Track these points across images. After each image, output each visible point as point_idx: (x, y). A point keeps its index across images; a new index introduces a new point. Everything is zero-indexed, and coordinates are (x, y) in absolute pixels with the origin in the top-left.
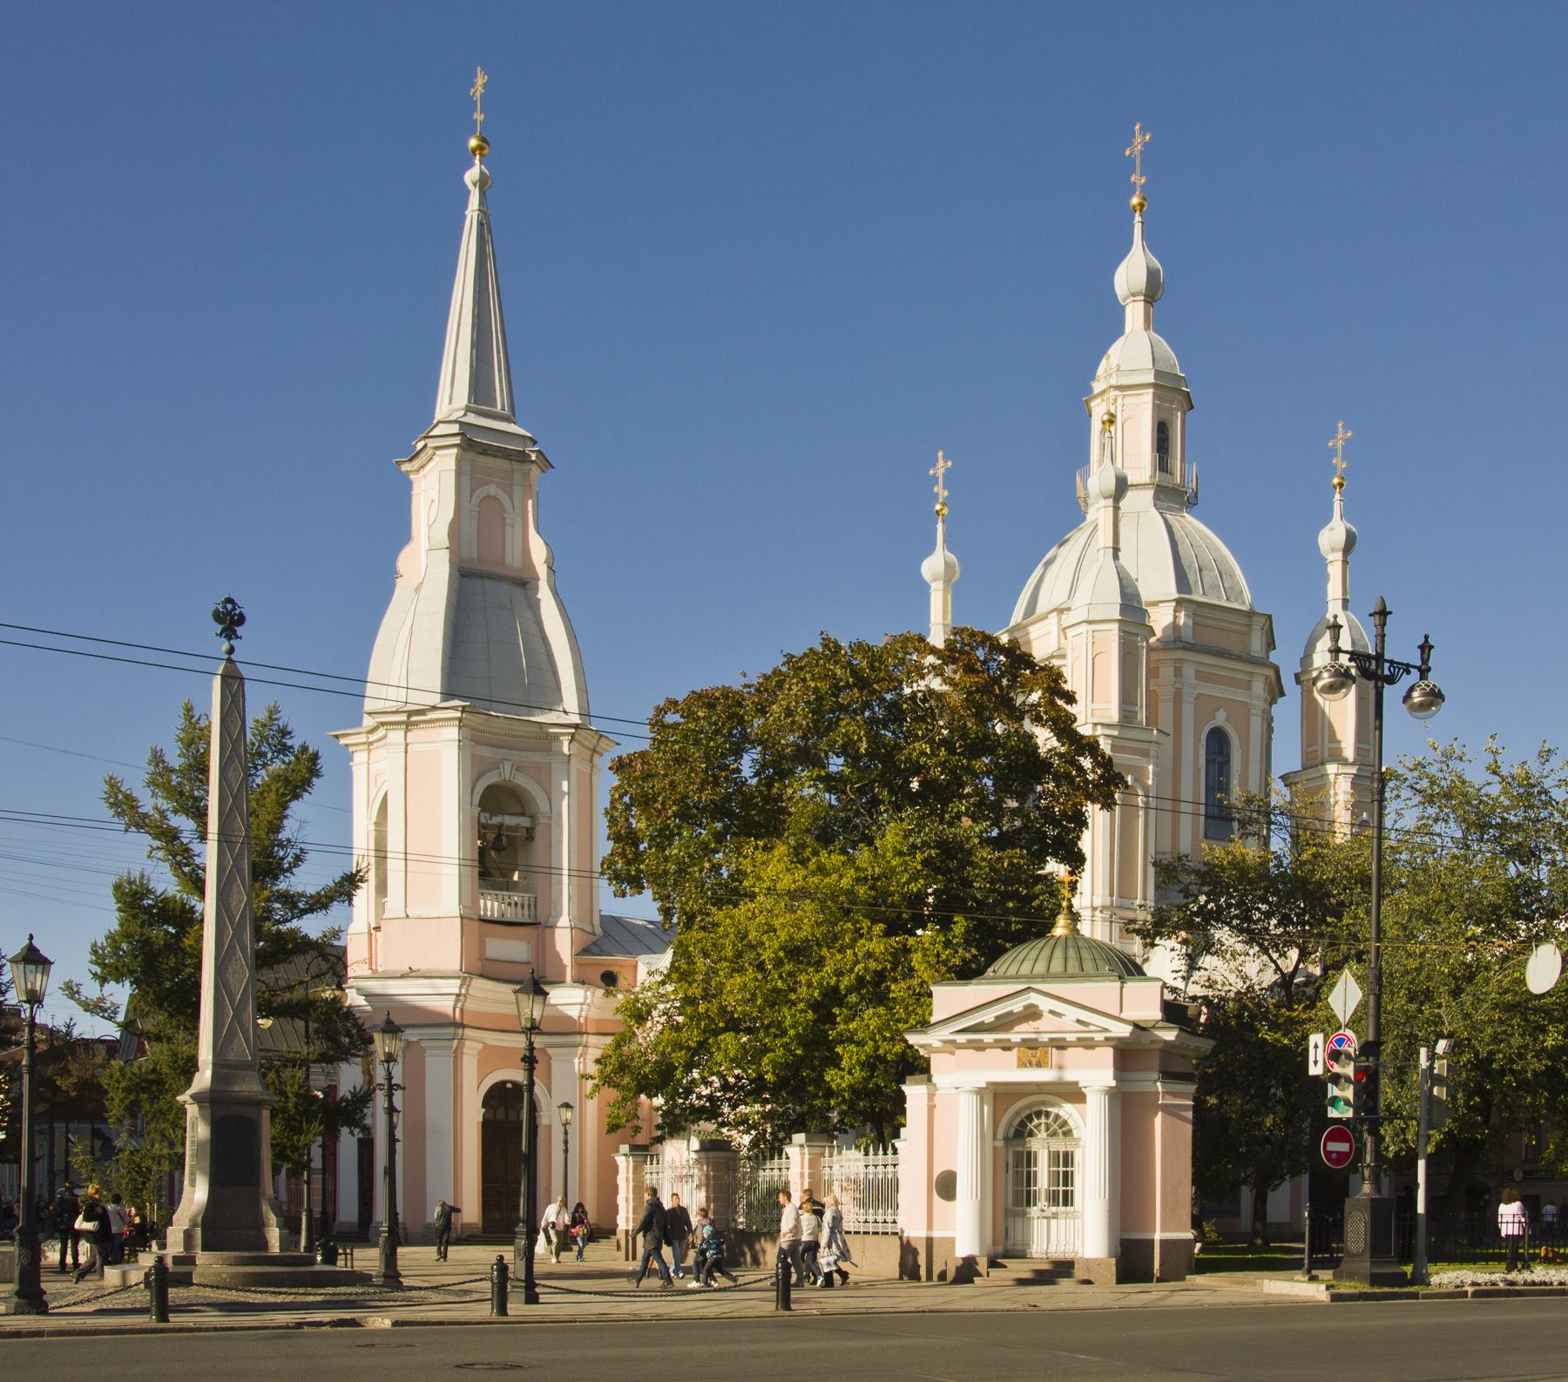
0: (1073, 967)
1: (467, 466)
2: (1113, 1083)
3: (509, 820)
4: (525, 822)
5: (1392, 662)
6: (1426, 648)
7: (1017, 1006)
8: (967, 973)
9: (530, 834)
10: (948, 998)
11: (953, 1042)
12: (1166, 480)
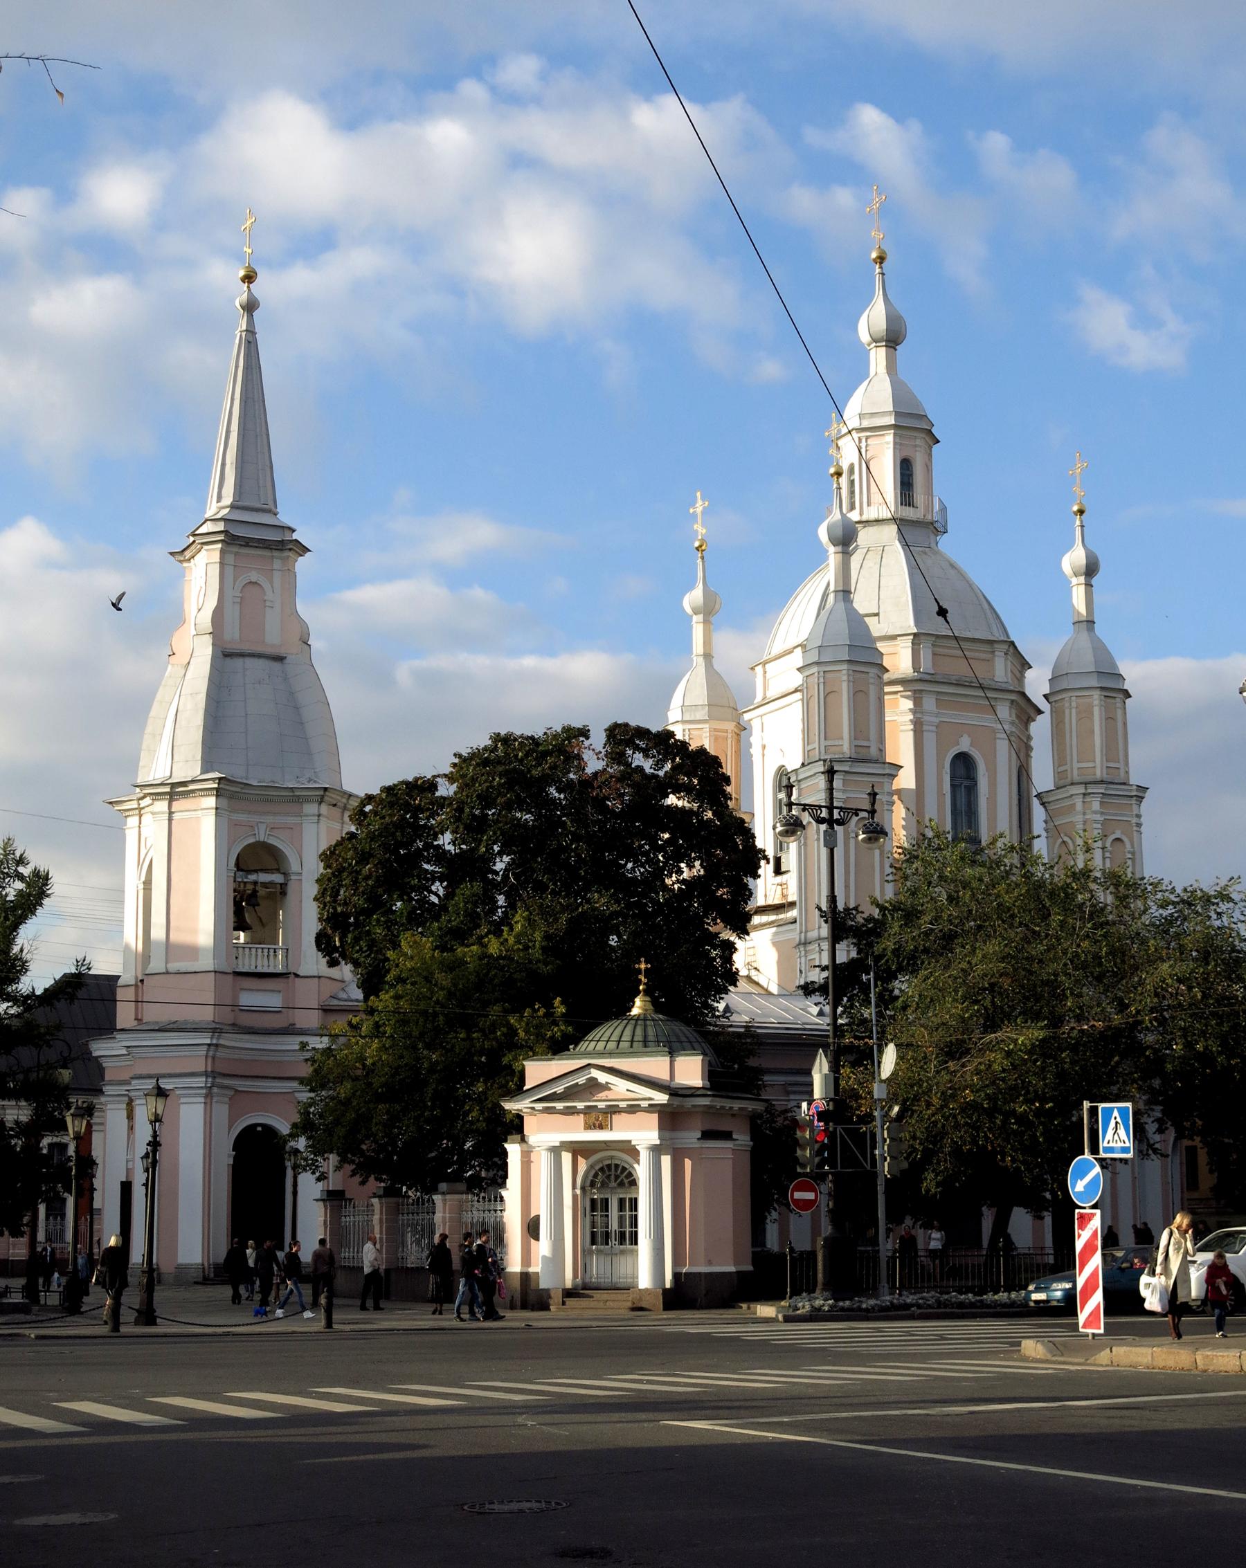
2: (658, 1142)
3: (264, 878)
4: (277, 878)
5: (841, 808)
7: (581, 1080)
8: (558, 1048)
9: (283, 890)
10: (537, 1071)
11: (533, 1108)
12: (909, 513)
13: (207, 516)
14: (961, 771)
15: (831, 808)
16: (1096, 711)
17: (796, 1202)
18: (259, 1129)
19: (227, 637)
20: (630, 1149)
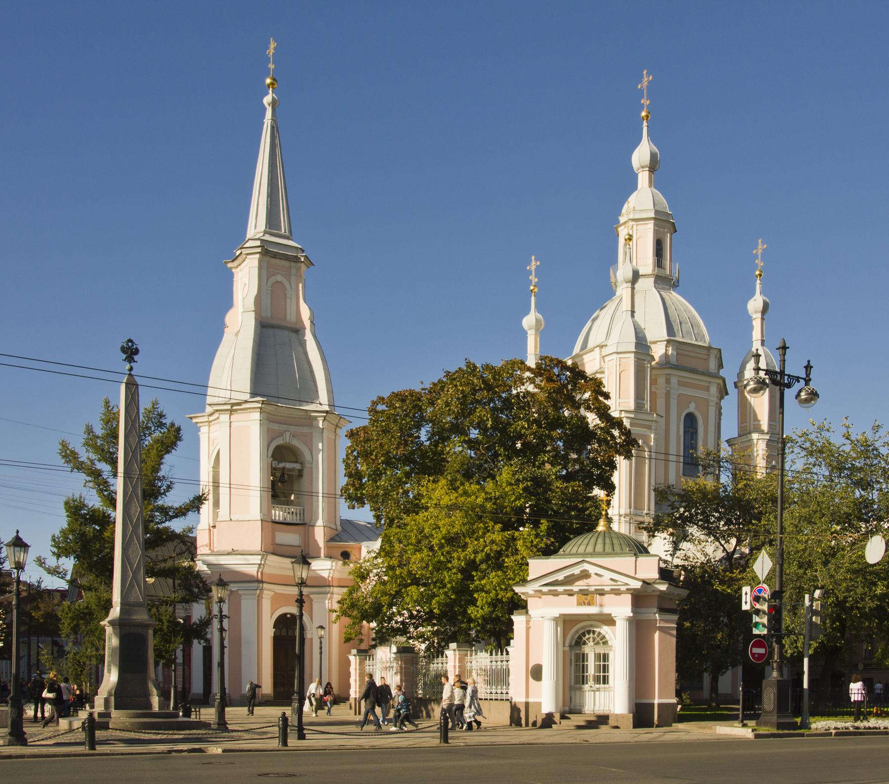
0: (608, 548)
1: (265, 265)
2: (631, 615)
3: (289, 465)
4: (297, 466)
5: (789, 376)
6: (808, 368)
7: (576, 571)
8: (548, 552)
9: (300, 473)
10: (538, 566)
11: (540, 591)
12: (661, 272)
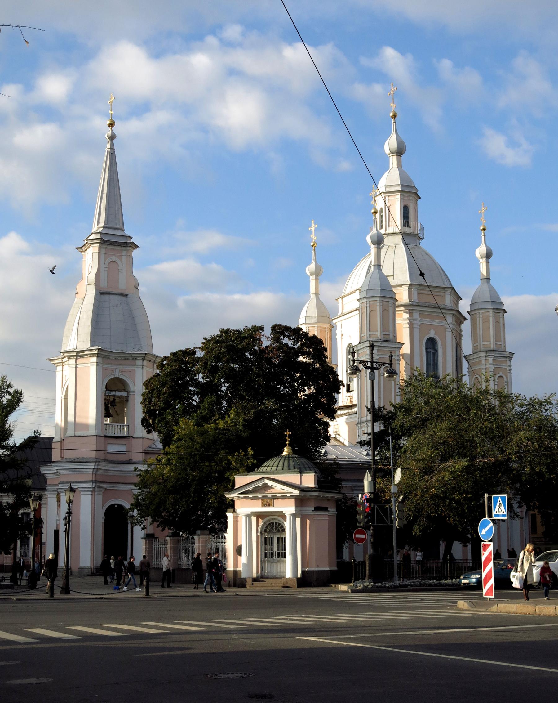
2: (295, 512)
3: (118, 393)
4: (124, 394)
5: (377, 362)
7: (260, 484)
8: (250, 470)
9: (127, 399)
10: (241, 480)
11: (239, 497)
12: (407, 230)
13: (93, 231)
14: (431, 346)
15: (372, 362)
16: (491, 319)
17: (357, 539)
18: (116, 506)
19: (102, 286)
20: (282, 515)
